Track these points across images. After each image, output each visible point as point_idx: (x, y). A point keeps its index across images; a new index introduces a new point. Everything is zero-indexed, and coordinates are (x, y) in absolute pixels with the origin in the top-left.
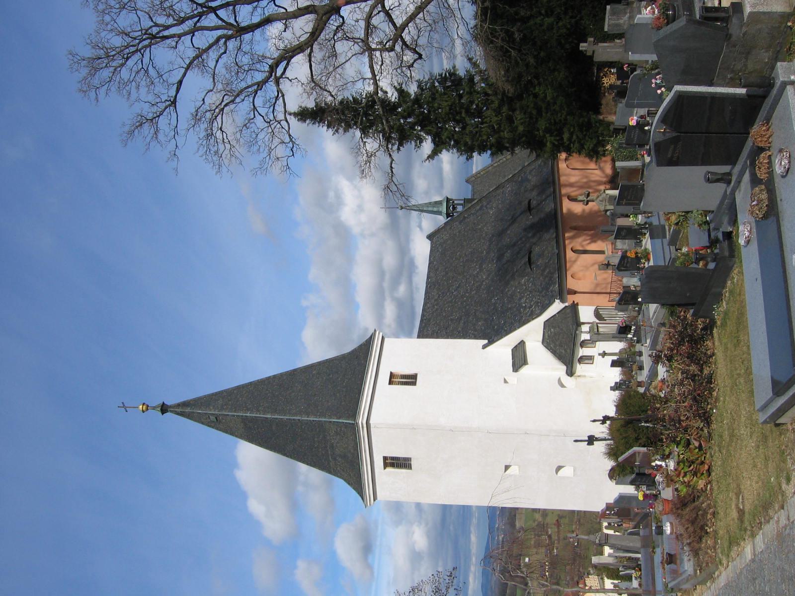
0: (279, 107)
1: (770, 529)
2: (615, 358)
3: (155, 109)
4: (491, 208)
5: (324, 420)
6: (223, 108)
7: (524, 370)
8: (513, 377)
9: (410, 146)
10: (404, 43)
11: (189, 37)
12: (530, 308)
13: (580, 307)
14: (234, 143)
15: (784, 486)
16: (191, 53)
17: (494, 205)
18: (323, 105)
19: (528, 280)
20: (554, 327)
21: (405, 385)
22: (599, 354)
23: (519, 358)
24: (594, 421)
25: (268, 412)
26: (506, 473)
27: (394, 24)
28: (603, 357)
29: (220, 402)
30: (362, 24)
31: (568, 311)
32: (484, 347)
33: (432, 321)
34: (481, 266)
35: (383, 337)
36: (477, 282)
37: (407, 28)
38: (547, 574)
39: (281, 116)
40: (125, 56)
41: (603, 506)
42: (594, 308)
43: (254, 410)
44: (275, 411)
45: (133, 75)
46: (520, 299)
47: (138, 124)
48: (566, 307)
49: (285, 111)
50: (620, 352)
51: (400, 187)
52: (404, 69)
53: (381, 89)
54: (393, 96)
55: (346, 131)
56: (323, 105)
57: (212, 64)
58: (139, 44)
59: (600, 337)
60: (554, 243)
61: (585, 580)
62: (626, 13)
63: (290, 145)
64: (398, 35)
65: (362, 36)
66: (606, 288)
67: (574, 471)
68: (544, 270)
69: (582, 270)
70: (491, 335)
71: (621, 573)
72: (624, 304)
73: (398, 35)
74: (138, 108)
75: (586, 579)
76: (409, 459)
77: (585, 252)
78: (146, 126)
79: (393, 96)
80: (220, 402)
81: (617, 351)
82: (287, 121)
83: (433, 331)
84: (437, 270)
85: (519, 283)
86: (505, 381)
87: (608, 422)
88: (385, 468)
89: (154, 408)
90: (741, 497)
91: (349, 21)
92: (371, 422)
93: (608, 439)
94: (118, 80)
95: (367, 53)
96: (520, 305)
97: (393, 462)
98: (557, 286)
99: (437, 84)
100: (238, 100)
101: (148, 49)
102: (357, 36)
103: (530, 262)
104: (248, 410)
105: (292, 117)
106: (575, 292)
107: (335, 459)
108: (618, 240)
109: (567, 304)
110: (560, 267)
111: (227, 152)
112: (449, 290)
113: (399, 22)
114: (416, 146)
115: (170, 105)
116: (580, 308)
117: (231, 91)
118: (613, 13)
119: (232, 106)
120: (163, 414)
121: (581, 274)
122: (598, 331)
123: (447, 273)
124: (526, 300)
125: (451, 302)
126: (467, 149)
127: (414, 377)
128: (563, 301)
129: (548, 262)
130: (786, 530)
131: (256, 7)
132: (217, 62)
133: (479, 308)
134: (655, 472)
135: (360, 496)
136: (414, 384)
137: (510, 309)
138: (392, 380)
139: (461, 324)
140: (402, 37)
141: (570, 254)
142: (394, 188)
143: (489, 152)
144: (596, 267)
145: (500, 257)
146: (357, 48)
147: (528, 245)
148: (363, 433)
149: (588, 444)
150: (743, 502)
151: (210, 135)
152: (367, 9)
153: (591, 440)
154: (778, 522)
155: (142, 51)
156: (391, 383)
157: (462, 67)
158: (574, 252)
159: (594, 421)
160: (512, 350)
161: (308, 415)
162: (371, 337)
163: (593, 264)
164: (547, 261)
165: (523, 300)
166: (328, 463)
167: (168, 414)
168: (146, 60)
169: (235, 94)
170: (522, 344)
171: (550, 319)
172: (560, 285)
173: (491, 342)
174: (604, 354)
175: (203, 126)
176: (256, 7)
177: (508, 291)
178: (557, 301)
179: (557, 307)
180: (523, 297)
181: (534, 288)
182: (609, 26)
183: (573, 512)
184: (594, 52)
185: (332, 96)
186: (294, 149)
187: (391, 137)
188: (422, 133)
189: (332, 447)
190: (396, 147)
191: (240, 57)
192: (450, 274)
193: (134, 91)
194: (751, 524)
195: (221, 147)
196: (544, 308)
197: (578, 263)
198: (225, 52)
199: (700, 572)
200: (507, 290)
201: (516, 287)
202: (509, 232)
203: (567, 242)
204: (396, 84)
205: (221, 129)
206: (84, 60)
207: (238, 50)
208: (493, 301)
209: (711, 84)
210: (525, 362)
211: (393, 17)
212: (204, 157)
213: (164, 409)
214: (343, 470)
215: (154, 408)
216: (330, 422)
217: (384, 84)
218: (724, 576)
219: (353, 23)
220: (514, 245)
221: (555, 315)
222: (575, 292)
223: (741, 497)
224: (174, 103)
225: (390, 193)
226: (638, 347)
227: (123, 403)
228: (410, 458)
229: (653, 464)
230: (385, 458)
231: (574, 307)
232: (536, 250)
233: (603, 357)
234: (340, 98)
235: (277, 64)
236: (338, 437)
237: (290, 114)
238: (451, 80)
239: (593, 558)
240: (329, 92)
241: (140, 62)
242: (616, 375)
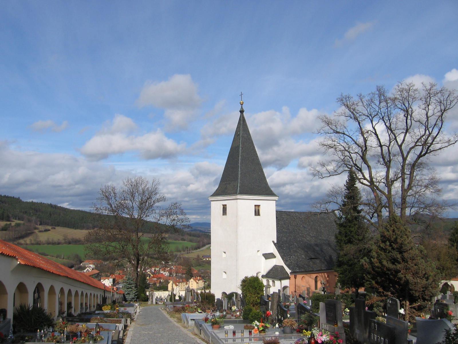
5: (239, 180)
7: (263, 258)
8: (260, 254)
12: (290, 260)
13: (289, 280)
20: (280, 270)
21: (255, 210)
23: (268, 256)
25: (241, 157)
26: (223, 252)
29: (245, 136)
32: (273, 242)
33: (289, 217)
34: (313, 237)
36: (306, 236)
38: (205, 259)
42: (289, 286)
43: (242, 151)
44: (242, 160)
46: (294, 255)
48: (288, 275)
59: (266, 288)
60: (319, 269)
61: (201, 280)
66: (298, 290)
67: (225, 279)
68: (307, 265)
69: (306, 281)
70: (279, 245)
75: (202, 281)
77: (316, 282)
80: (245, 136)
83: (284, 218)
85: (302, 254)
86: (258, 251)
88: (222, 205)
89: (242, 107)
92: (238, 200)
96: (292, 255)
97: (225, 208)
98: (298, 271)
103: (311, 259)
104: (242, 148)
106: (295, 278)
109: (289, 275)
110: (306, 271)
112: (303, 223)
116: (288, 280)
121: (304, 280)
122: (268, 288)
123: (312, 221)
124: (294, 258)
125: (297, 224)
127: (259, 215)
128: (291, 273)
129: (310, 267)
133: (293, 237)
136: (256, 215)
138: (257, 206)
139: (285, 230)
141: (314, 276)
144: (308, 286)
145: (317, 245)
147: (321, 257)
148: (234, 197)
156: (255, 206)
158: (315, 277)
160: (272, 253)
161: (241, 174)
163: (309, 285)
164: (311, 266)
165: (294, 257)
167: (240, 114)
170: (275, 257)
171: (284, 268)
172: (297, 272)
173: (275, 244)
177: (299, 250)
178: (291, 271)
179: (288, 271)
181: (299, 261)
192: (312, 223)
196: (288, 266)
197: (310, 279)
200: (300, 249)
202: (329, 248)
203: (320, 274)
208: (295, 244)
210: (266, 258)
213: (242, 112)
215: (242, 107)
216: (238, 183)
220: (322, 251)
221: (285, 270)
222: (295, 278)
228: (226, 215)
231: (288, 278)
232: (318, 261)
236: (233, 186)
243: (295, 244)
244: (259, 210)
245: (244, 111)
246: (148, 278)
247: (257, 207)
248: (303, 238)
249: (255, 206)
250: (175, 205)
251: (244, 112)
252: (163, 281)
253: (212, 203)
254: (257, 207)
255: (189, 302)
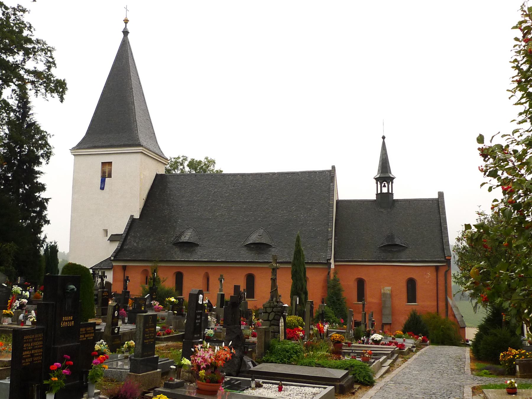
42: (112, 283)
213: (126, 33)
247: (107, 165)
251: (129, 34)
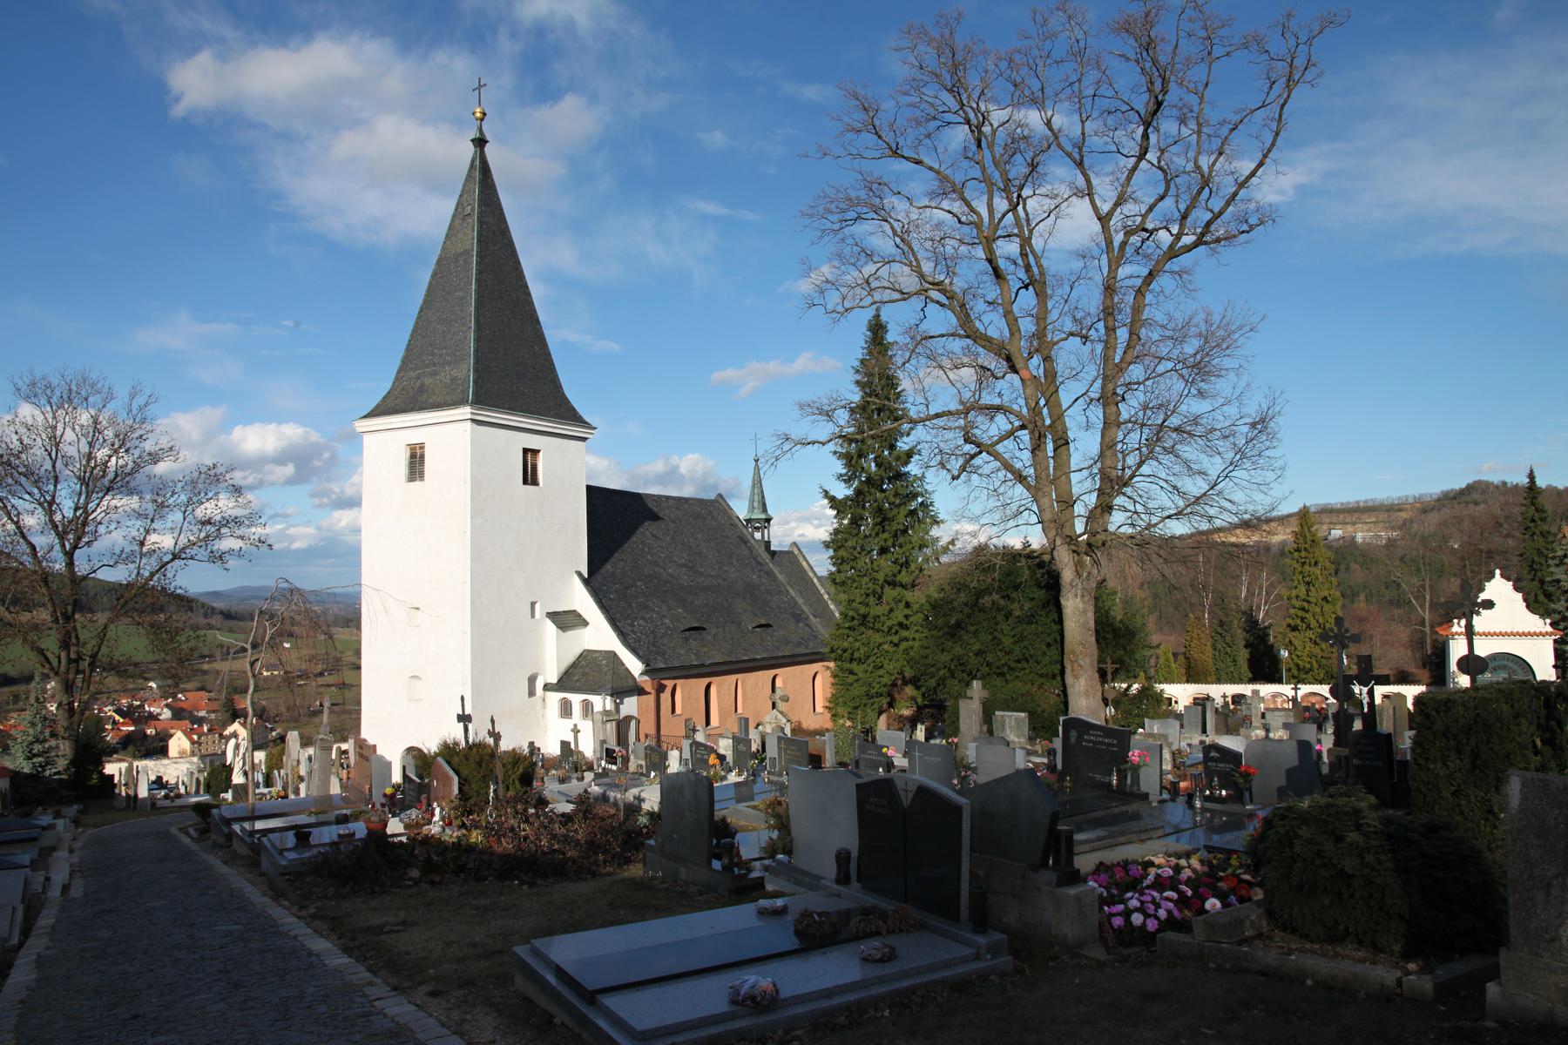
0: (888, 295)
1: (359, 973)
2: (573, 746)
3: (885, 127)
4: (760, 576)
6: (886, 221)
9: (839, 467)
10: (973, 457)
11: (978, 174)
12: (633, 631)
14: (840, 236)
15: (423, 989)
16: (959, 178)
17: (764, 580)
18: (890, 353)
19: (668, 628)
22: (575, 725)
24: (493, 721)
27: (997, 443)
28: (572, 730)
30: (997, 401)
31: (630, 682)
32: (579, 574)
34: (682, 566)
35: (587, 439)
37: (992, 458)
39: (877, 297)
40: (955, 89)
41: (371, 742)
42: (635, 714)
45: (930, 100)
46: (643, 618)
47: (866, 105)
49: (882, 302)
50: (580, 752)
51: (788, 455)
52: (939, 457)
53: (912, 429)
54: (903, 444)
55: (858, 383)
56: (890, 353)
57: (945, 204)
58: (972, 108)
62: (1019, 737)
63: (840, 309)
64: (982, 447)
65: (982, 402)
71: (276, 772)
72: (646, 754)
73: (982, 447)
74: (888, 105)
76: (422, 477)
78: (862, 116)
79: (903, 444)
81: (581, 749)
82: (872, 304)
84: (678, 509)
87: (491, 741)
89: (481, 129)
90: (400, 928)
91: (1000, 384)
93: (467, 742)
94: (925, 78)
95: (961, 407)
96: (635, 619)
98: (663, 666)
99: (920, 500)
100: (898, 240)
101: (962, 121)
102: (983, 395)
105: (873, 313)
107: (418, 377)
108: (731, 741)
111: (829, 225)
113: (1000, 448)
114: (841, 475)
115: (891, 148)
117: (908, 232)
118: (1018, 721)
119: (890, 232)
120: (472, 141)
123: (673, 522)
126: (836, 542)
127: (535, 482)
130: (361, 996)
131: (1015, 263)
132: (949, 212)
134: (424, 808)
135: (372, 411)
136: (525, 482)
137: (630, 606)
140: (980, 452)
142: (786, 448)
143: (834, 569)
146: (967, 395)
149: (458, 715)
150: (393, 931)
151: (852, 202)
152: (1016, 407)
153: (464, 719)
154: (371, 984)
155: (961, 112)
156: (526, 451)
157: (941, 534)
159: (493, 721)
162: (585, 422)
165: (642, 623)
166: (411, 369)
168: (950, 117)
169: (905, 236)
174: (576, 731)
175: (863, 194)
176: (1015, 263)
179: (635, 666)
180: (646, 622)
181: (660, 635)
182: (1002, 716)
183: (359, 703)
184: (972, 698)
185: (904, 364)
186: (834, 315)
187: (850, 444)
188: (856, 483)
189: (435, 374)
190: (839, 449)
191: (951, 243)
193: (908, 99)
194: (363, 945)
195: (834, 218)
198: (960, 222)
199: (287, 880)
201: (658, 613)
204: (919, 447)
205: (859, 217)
206: (951, 33)
207: (960, 240)
208: (639, 583)
209: (972, 849)
211: (1005, 442)
212: (822, 195)
213: (480, 142)
214: (403, 390)
215: (481, 129)
217: (920, 433)
218: (285, 918)
219: (997, 391)
223: (400, 928)
224: (895, 153)
225: (779, 442)
226: (589, 776)
227: (485, 85)
229: (435, 805)
230: (422, 446)
233: (572, 730)
234: (900, 374)
235: (943, 292)
237: (878, 310)
238: (923, 515)
239: (296, 733)
240: (909, 360)
241: (946, 109)
242: (552, 749)
243: (639, 583)
244: (534, 468)
245: (487, 142)
246: (109, 727)
247: (530, 454)
248: (657, 569)
249: (526, 451)
250: (212, 473)
252: (154, 732)
253: (368, 440)
254: (530, 454)
255: (330, 797)
